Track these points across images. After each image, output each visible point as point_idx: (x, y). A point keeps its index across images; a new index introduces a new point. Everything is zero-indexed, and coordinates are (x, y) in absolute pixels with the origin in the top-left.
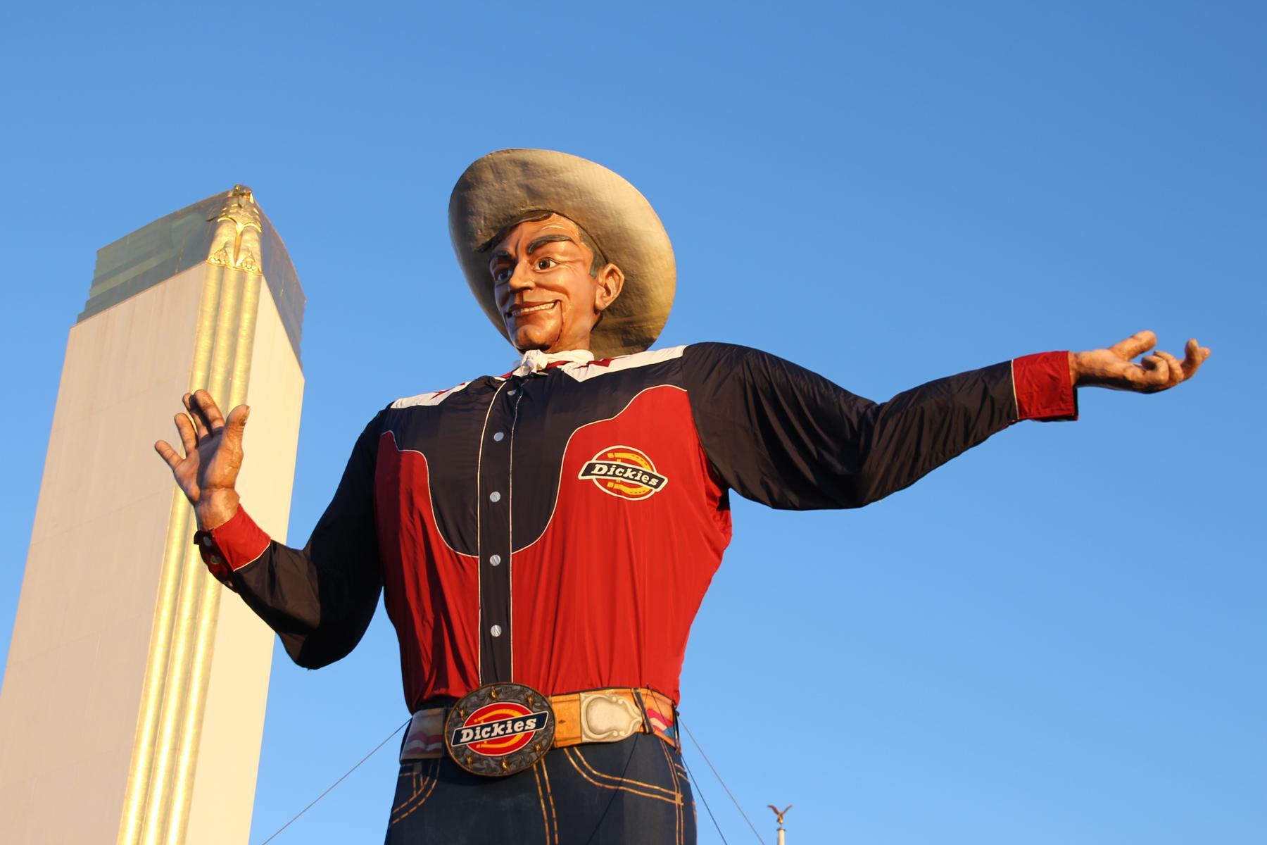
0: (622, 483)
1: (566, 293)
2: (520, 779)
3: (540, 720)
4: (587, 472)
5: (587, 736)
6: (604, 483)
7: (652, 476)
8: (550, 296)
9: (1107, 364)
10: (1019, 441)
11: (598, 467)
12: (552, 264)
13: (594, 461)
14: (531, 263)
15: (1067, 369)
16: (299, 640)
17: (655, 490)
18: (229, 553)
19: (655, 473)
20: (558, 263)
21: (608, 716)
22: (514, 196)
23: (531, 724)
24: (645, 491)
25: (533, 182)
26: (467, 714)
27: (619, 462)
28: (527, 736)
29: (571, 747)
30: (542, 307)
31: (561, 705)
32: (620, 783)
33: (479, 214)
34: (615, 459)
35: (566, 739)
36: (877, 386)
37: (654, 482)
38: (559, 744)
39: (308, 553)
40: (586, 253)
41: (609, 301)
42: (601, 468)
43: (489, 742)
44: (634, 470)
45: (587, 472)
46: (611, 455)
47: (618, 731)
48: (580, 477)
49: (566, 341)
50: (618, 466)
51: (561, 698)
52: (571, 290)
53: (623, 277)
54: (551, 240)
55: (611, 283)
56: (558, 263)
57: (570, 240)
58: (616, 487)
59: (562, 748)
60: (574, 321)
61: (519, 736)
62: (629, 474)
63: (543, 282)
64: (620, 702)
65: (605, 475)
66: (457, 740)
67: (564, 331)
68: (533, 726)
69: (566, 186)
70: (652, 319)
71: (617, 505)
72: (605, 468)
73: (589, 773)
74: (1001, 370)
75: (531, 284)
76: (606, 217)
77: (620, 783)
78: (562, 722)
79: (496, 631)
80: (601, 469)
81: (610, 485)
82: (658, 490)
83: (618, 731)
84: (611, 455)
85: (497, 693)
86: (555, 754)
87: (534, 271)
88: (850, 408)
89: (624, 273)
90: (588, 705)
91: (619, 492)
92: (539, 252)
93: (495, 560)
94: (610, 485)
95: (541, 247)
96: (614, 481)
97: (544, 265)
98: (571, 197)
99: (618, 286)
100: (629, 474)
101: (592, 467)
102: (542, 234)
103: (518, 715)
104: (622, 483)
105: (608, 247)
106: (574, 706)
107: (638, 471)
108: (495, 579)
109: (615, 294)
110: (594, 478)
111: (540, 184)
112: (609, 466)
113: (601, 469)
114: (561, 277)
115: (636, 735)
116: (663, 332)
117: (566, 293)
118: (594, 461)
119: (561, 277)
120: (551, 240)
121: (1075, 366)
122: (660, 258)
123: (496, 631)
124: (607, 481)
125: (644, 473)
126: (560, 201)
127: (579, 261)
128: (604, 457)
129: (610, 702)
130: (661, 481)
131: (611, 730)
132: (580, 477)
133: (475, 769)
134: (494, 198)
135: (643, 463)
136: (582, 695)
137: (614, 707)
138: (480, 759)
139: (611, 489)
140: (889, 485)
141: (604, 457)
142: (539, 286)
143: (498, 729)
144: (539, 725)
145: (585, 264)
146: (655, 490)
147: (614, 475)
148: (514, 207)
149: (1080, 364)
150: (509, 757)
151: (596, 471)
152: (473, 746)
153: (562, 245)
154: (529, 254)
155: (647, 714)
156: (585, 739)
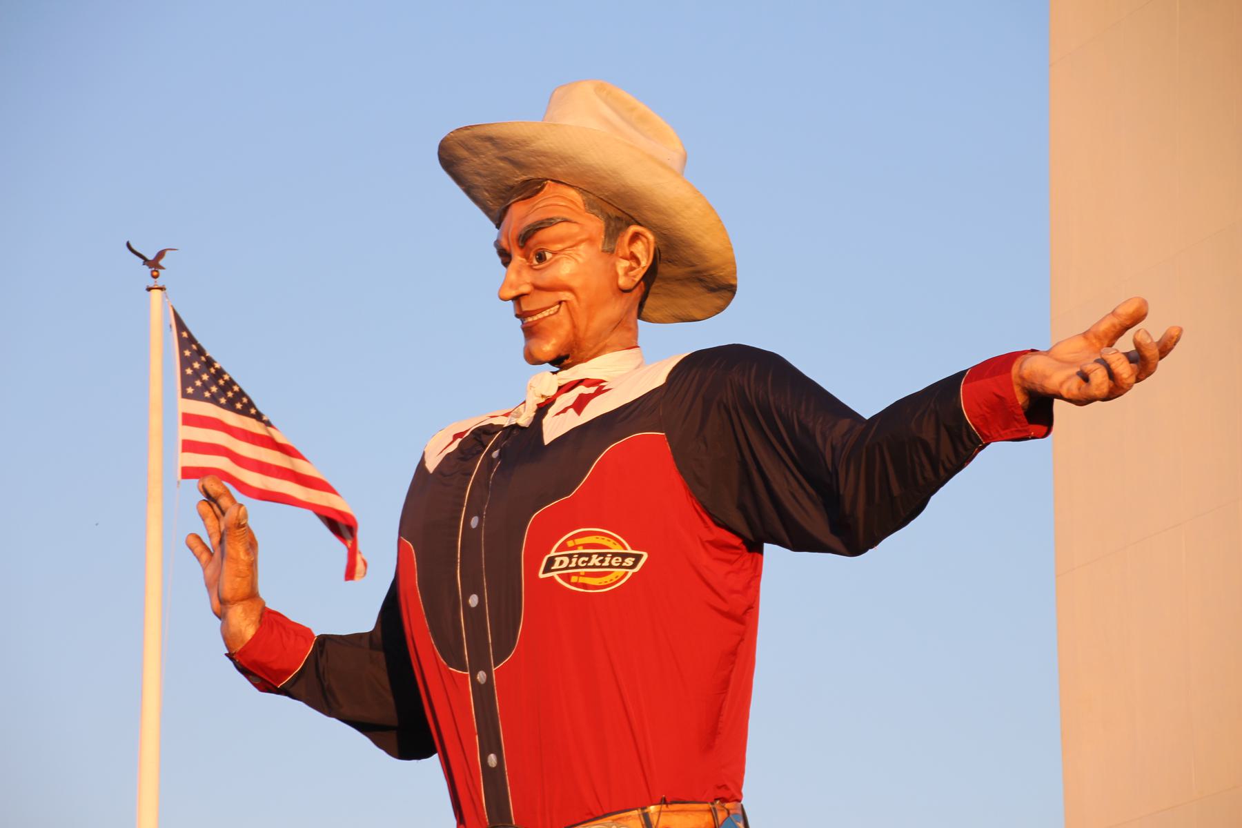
0: (587, 575)
4: (547, 570)
6: (567, 578)
8: (548, 298)
9: (1045, 377)
10: (997, 460)
11: (558, 560)
12: (548, 256)
13: (553, 554)
14: (527, 257)
15: (1010, 384)
16: (392, 737)
17: (631, 572)
18: (282, 662)
19: (630, 551)
20: (554, 253)
22: (500, 168)
24: (619, 575)
25: (508, 154)
27: (581, 550)
30: (546, 313)
33: (478, 187)
34: (575, 548)
37: (629, 561)
39: (379, 634)
40: (595, 225)
41: (639, 273)
42: (562, 561)
44: (600, 555)
45: (547, 570)
46: (570, 544)
48: (541, 576)
49: (588, 344)
50: (581, 555)
52: (575, 283)
53: (651, 237)
55: (639, 248)
56: (554, 253)
58: (582, 580)
60: (590, 318)
62: (595, 560)
63: (540, 283)
65: (567, 568)
67: (581, 335)
71: (584, 603)
72: (566, 560)
74: (949, 385)
75: (525, 289)
76: (604, 178)
80: (562, 562)
81: (574, 579)
82: (636, 570)
84: (570, 544)
87: (531, 267)
88: (825, 441)
89: (654, 234)
91: (585, 586)
92: (532, 242)
93: (481, 676)
94: (574, 579)
96: (577, 574)
97: (541, 258)
98: (556, 165)
99: (648, 251)
100: (595, 560)
101: (551, 561)
104: (587, 575)
105: (620, 212)
107: (604, 555)
109: (645, 263)
110: (554, 574)
111: (518, 155)
112: (570, 556)
113: (562, 562)
116: (739, 275)
118: (553, 554)
121: (1019, 381)
124: (569, 575)
125: (614, 555)
127: (582, 241)
128: (563, 547)
132: (541, 576)
134: (483, 172)
135: (610, 543)
139: (576, 585)
141: (563, 547)
142: (537, 288)
145: (591, 240)
146: (631, 572)
147: (577, 567)
148: (507, 178)
149: (1022, 378)
151: (556, 566)
154: (521, 248)
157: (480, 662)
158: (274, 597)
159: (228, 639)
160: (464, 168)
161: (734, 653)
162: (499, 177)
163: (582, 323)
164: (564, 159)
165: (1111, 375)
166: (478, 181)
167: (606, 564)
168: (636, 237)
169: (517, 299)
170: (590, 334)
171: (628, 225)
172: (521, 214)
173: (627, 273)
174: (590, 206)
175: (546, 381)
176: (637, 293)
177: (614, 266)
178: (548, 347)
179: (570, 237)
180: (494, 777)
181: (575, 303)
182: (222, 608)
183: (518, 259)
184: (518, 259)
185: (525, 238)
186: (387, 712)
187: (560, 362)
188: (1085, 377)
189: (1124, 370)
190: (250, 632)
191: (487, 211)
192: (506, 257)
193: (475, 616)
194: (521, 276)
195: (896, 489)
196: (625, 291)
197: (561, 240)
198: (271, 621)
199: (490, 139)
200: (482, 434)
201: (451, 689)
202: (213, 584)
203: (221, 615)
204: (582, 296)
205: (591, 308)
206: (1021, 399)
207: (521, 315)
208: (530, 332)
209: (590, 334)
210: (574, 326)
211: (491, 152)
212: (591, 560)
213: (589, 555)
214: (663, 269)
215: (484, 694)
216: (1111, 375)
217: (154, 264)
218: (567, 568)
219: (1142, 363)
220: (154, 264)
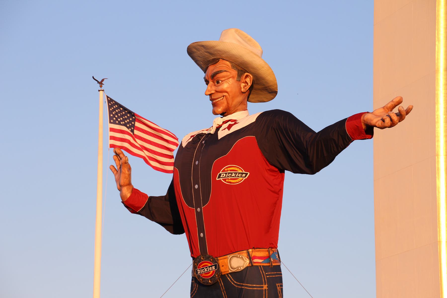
0: (231, 179)
1: (227, 92)
2: (215, 285)
3: (216, 266)
5: (231, 270)
7: (242, 174)
8: (220, 95)
9: (371, 120)
11: (222, 174)
12: (220, 82)
13: (221, 173)
14: (214, 82)
17: (244, 178)
18: (137, 204)
19: (244, 172)
20: (222, 81)
21: (237, 262)
23: (214, 267)
24: (241, 180)
25: (208, 50)
26: (197, 265)
27: (229, 172)
28: (213, 271)
29: (227, 274)
31: (222, 261)
32: (242, 286)
34: (227, 171)
35: (225, 272)
36: (317, 125)
37: (244, 175)
38: (223, 274)
40: (234, 73)
41: (248, 87)
43: (205, 274)
44: (235, 173)
47: (240, 267)
48: (217, 179)
50: (229, 173)
51: (222, 258)
52: (228, 90)
53: (252, 76)
54: (220, 72)
55: (248, 80)
56: (222, 81)
57: (226, 71)
58: (229, 181)
59: (225, 275)
60: (233, 101)
61: (212, 272)
63: (217, 90)
64: (241, 257)
65: (225, 177)
66: (197, 274)
67: (230, 106)
68: (214, 268)
69: (219, 51)
70: (271, 86)
71: (230, 188)
72: (225, 175)
73: (234, 282)
75: (213, 92)
77: (242, 286)
78: (223, 266)
79: (202, 235)
81: (227, 180)
82: (246, 178)
83: (240, 267)
84: (226, 170)
85: (203, 258)
86: (223, 277)
87: (215, 85)
90: (230, 259)
91: (230, 183)
92: (215, 78)
93: (199, 210)
94: (227, 180)
95: (215, 76)
96: (228, 179)
97: (218, 82)
99: (251, 81)
100: (233, 175)
101: (220, 175)
102: (215, 71)
103: (210, 265)
104: (231, 179)
105: (242, 68)
106: (225, 260)
107: (236, 173)
108: (199, 215)
110: (221, 179)
111: (211, 51)
112: (226, 174)
114: (225, 86)
115: (247, 267)
117: (227, 92)
118: (221, 173)
119: (225, 86)
120: (220, 72)
122: (263, 67)
123: (202, 235)
125: (239, 173)
126: (220, 56)
127: (230, 77)
129: (237, 257)
130: (247, 174)
131: (238, 267)
132: (217, 179)
133: (204, 283)
136: (228, 256)
137: (239, 259)
138: (203, 279)
140: (339, 149)
142: (217, 92)
143: (206, 270)
144: (216, 268)
145: (233, 77)
146: (244, 178)
147: (228, 177)
150: (211, 278)
151: (222, 176)
152: (201, 275)
153: (224, 74)
154: (212, 79)
155: (251, 258)
156: (230, 272)
157: (198, 205)
158: (136, 184)
159: (122, 197)
160: (195, 55)
161: (276, 203)
162: (205, 57)
163: (230, 102)
164: (225, 52)
165: (391, 120)
166: (199, 59)
167: (237, 176)
168: (247, 76)
169: (210, 95)
170: (232, 106)
171: (245, 73)
172: (212, 69)
173: (244, 87)
174: (233, 67)
175: (219, 120)
176: (247, 93)
177: (240, 85)
178: (220, 110)
179: (227, 76)
180: (202, 240)
181: (228, 96)
182: (120, 188)
183: (211, 83)
184: (211, 83)
185: (213, 76)
186: (170, 220)
187: (223, 114)
188: (383, 120)
189: (395, 118)
190: (129, 195)
191: (202, 68)
192: (207, 82)
193: (197, 191)
194: (212, 88)
195: (325, 154)
196: (243, 93)
197: (224, 77)
198: (135, 192)
199: (203, 46)
200: (200, 136)
201: (189, 212)
202: (118, 180)
203: (120, 190)
204: (230, 94)
205: (233, 98)
206: (364, 127)
207: (212, 100)
208: (214, 105)
209: (232, 106)
210: (228, 103)
211: (203, 50)
212: (232, 175)
213: (232, 173)
214: (255, 86)
215: (199, 215)
216: (391, 120)
217: (101, 83)
218: (225, 177)
219: (401, 117)
220: (101, 83)
